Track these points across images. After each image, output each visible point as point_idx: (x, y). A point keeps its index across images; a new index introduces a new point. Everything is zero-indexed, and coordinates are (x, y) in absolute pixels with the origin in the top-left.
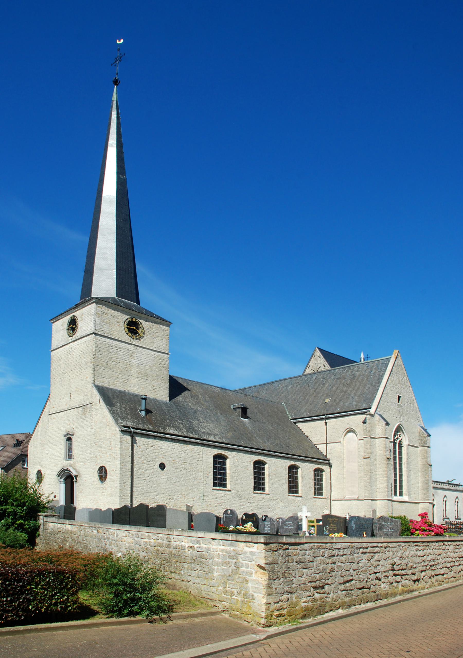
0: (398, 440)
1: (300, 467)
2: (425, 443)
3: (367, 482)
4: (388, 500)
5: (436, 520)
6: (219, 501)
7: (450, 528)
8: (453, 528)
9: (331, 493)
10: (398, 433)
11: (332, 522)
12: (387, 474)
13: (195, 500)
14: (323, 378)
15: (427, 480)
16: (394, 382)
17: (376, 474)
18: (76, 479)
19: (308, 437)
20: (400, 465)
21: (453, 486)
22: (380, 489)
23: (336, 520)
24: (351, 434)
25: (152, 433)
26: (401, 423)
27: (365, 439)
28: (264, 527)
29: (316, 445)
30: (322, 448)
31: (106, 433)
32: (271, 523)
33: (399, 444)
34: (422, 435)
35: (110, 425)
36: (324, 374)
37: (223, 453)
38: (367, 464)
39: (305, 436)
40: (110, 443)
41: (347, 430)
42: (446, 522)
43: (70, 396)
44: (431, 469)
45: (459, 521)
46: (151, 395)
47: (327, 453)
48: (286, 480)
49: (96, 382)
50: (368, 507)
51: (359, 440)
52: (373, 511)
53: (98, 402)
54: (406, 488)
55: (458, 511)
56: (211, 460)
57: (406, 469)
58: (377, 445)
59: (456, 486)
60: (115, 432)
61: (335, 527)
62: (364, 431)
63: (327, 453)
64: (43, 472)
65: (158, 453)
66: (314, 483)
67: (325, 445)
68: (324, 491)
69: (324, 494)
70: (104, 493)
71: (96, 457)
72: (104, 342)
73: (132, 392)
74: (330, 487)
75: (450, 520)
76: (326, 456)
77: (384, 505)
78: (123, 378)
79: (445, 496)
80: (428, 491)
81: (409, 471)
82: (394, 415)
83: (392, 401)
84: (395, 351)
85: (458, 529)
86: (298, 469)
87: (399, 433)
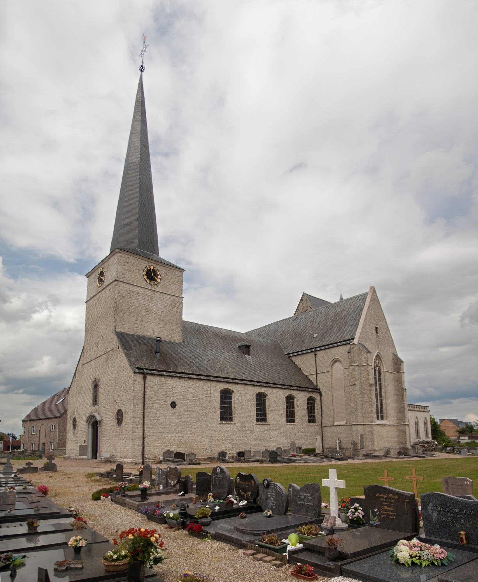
0: (378, 367)
3: (355, 408)
6: (226, 435)
11: (385, 502)
13: (204, 436)
18: (100, 423)
19: (300, 369)
23: (393, 499)
24: (337, 365)
25: (164, 373)
27: (350, 367)
28: (267, 498)
30: (313, 378)
31: (123, 377)
32: (276, 493)
33: (378, 371)
35: (126, 368)
37: (229, 388)
40: (126, 386)
43: (97, 345)
46: (165, 337)
47: (317, 382)
48: (284, 410)
49: (117, 329)
51: (345, 369)
53: (117, 348)
56: (218, 396)
60: (130, 374)
61: (392, 511)
63: (317, 382)
64: (77, 419)
65: (170, 392)
66: (308, 411)
67: (318, 375)
68: (316, 418)
70: (120, 437)
71: (115, 401)
72: (125, 288)
73: (150, 336)
76: (317, 385)
77: (369, 430)
78: (142, 324)
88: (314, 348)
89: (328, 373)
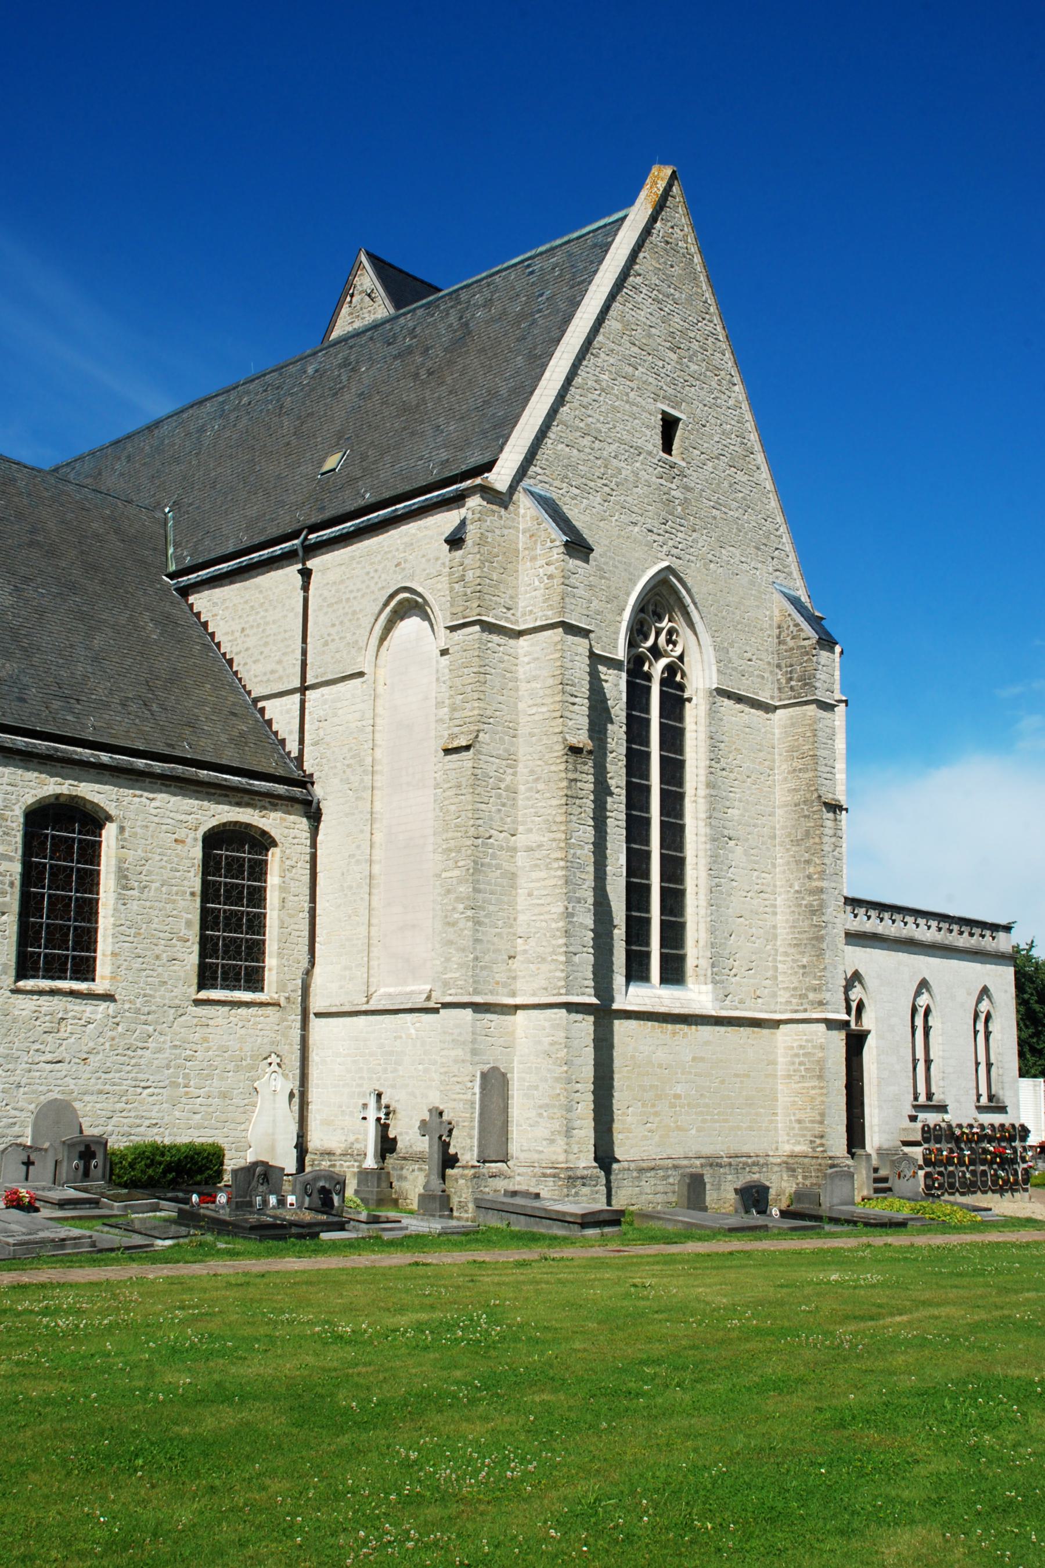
0: (663, 662)
1: (113, 812)
2: (807, 681)
4: (571, 1007)
5: (876, 1121)
7: (949, 1161)
8: (961, 1163)
9: (309, 973)
10: (660, 619)
12: (569, 846)
14: (346, 363)
15: (812, 892)
16: (639, 333)
17: (514, 849)
19: (230, 662)
20: (673, 803)
21: (966, 929)
22: (532, 942)
24: (411, 625)
26: (676, 564)
29: (260, 705)
33: (663, 682)
34: (791, 643)
36: (351, 347)
38: (459, 786)
39: (215, 660)
41: (393, 603)
42: (926, 1130)
44: (837, 828)
45: (997, 1119)
47: (301, 741)
50: (459, 1052)
52: (484, 1075)
54: (703, 936)
55: (989, 1065)
57: (703, 830)
58: (522, 672)
59: (977, 931)
62: (452, 589)
63: (301, 741)
68: (271, 961)
69: (270, 977)
74: (306, 941)
75: (947, 1117)
76: (300, 759)
79: (924, 985)
80: (820, 954)
81: (720, 838)
82: (634, 518)
83: (626, 437)
84: (655, 170)
85: (991, 1163)
86: (101, 827)
87: (665, 624)
88: (295, 535)
89: (358, 681)
